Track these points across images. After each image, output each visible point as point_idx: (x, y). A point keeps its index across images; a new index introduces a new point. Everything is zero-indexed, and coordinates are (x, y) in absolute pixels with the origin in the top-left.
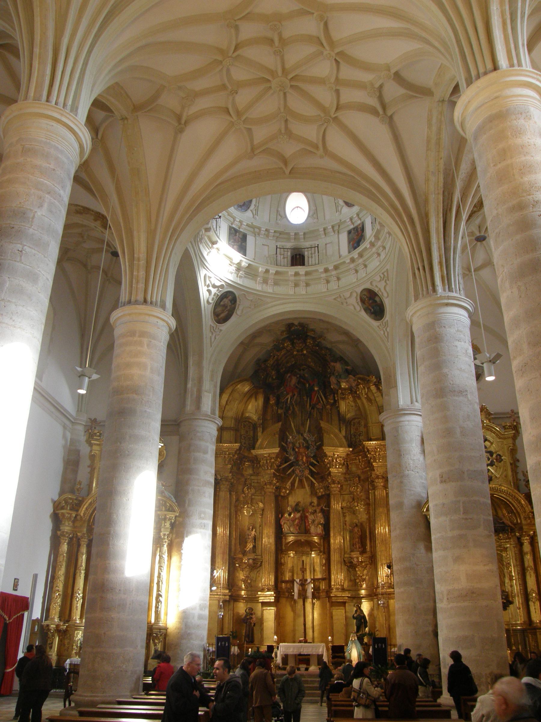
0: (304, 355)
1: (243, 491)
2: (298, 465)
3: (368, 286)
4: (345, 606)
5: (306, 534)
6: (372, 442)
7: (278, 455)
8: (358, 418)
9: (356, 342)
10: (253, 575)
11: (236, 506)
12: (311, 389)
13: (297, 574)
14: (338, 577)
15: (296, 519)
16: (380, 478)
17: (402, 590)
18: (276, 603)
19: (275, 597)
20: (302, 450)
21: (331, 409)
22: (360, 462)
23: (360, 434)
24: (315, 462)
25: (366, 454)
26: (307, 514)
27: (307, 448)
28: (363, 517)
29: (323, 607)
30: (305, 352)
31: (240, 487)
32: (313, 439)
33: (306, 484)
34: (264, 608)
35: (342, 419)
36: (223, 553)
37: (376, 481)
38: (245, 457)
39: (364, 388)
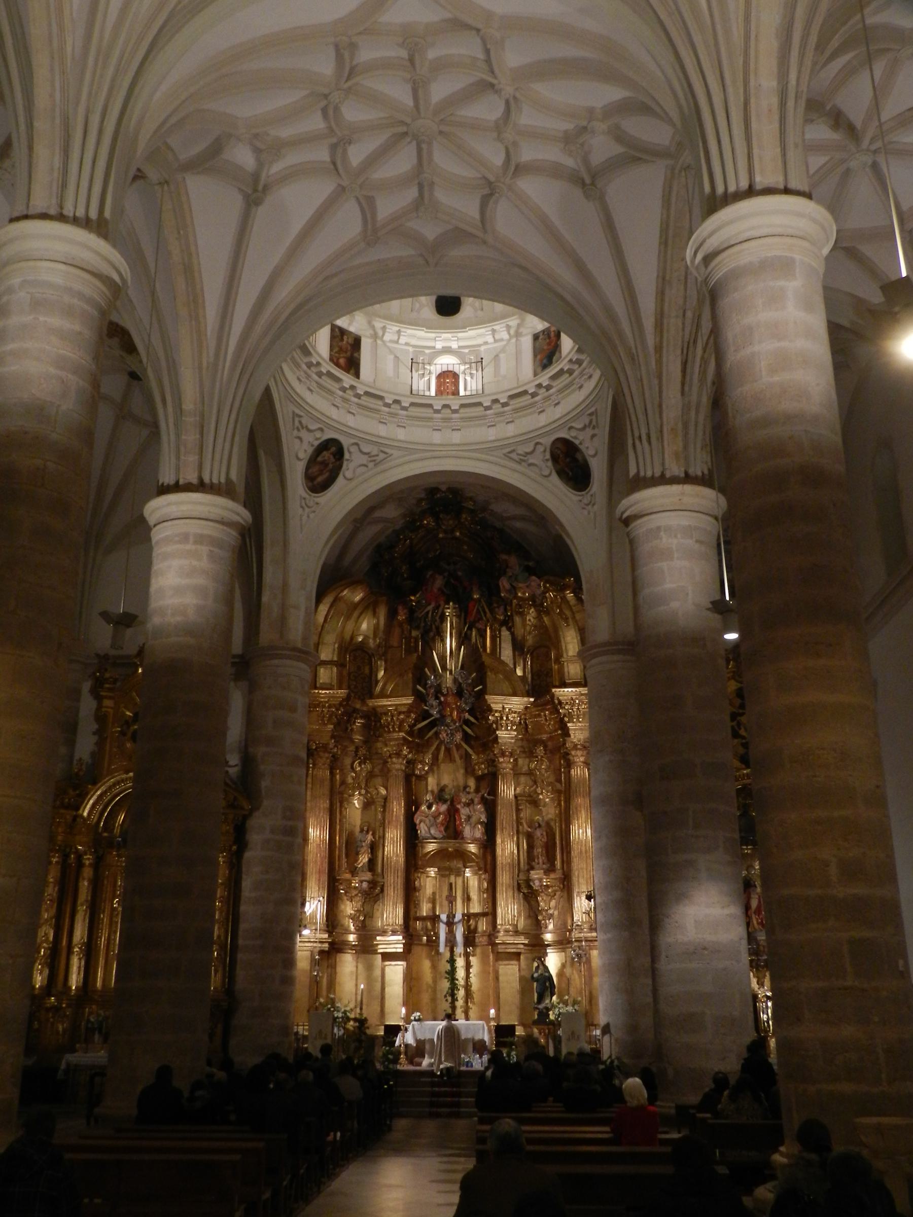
1: (352, 767)
4: (519, 960)
6: (566, 690)
7: (411, 709)
13: (441, 906)
14: (509, 910)
16: (580, 749)
19: (404, 944)
20: (450, 699)
22: (546, 720)
26: (459, 806)
29: (484, 961)
31: (348, 761)
34: (387, 963)
38: (355, 710)
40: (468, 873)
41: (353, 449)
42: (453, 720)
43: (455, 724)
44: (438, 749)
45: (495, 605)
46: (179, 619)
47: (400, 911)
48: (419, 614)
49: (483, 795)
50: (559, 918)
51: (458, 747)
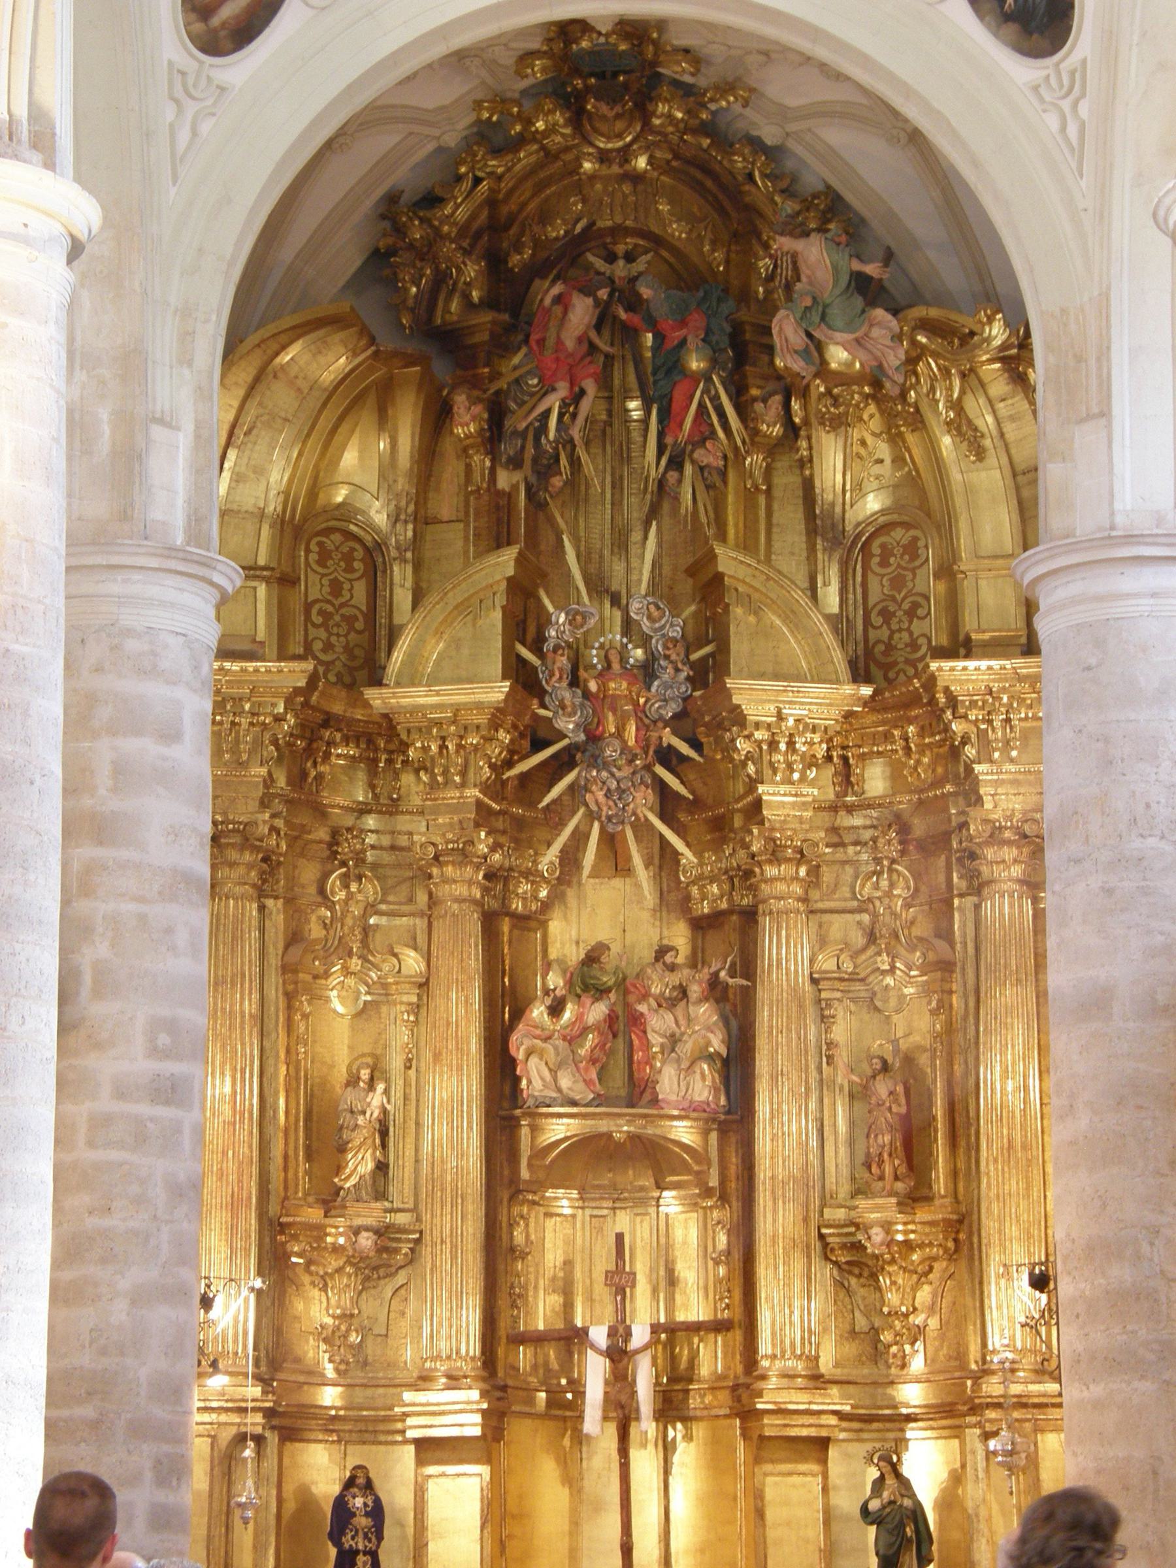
0: (637, 178)
1: (322, 891)
2: (596, 761)
4: (824, 1461)
6: (971, 664)
8: (907, 526)
10: (370, 1306)
12: (670, 363)
13: (590, 1300)
14: (795, 1312)
16: (1009, 843)
17: (1097, 1390)
18: (490, 1444)
19: (484, 1413)
20: (618, 686)
21: (768, 472)
22: (907, 749)
23: (915, 606)
24: (684, 749)
26: (642, 1008)
27: (648, 671)
28: (914, 1025)
29: (717, 1462)
31: (309, 873)
32: (676, 632)
34: (431, 1470)
35: (821, 525)
36: (234, 1206)
37: (990, 853)
38: (328, 721)
42: (625, 748)
43: (631, 762)
44: (579, 838)
45: (755, 392)
47: (472, 1318)
48: (519, 421)
50: (942, 1337)
51: (642, 829)
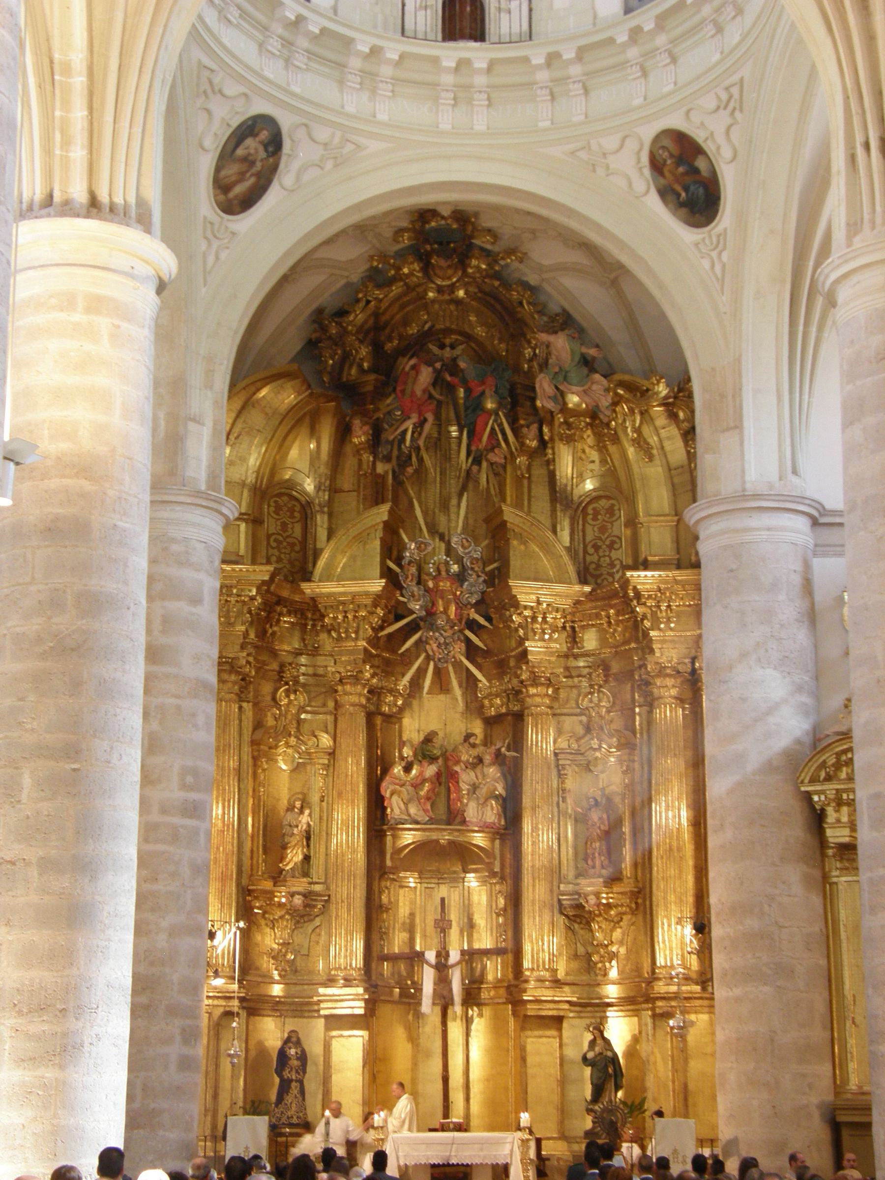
0: (458, 302)
1: (274, 699)
2: (432, 627)
3: (676, 122)
4: (560, 1029)
5: (449, 823)
7: (377, 599)
8: (608, 498)
9: (612, 273)
10: (299, 939)
11: (254, 743)
12: (475, 406)
13: (424, 936)
14: (544, 945)
15: (424, 781)
19: (366, 1001)
20: (445, 585)
21: (529, 468)
22: (609, 623)
23: (613, 542)
24: (482, 621)
25: (629, 605)
26: (457, 768)
27: (460, 578)
29: (497, 1029)
30: (461, 293)
33: (455, 683)
37: (658, 682)
38: (280, 601)
39: (632, 411)
40: (472, 880)
41: (301, 133)
44: (421, 673)
46: (64, 446)
47: (358, 945)
48: (390, 435)
49: (499, 750)
